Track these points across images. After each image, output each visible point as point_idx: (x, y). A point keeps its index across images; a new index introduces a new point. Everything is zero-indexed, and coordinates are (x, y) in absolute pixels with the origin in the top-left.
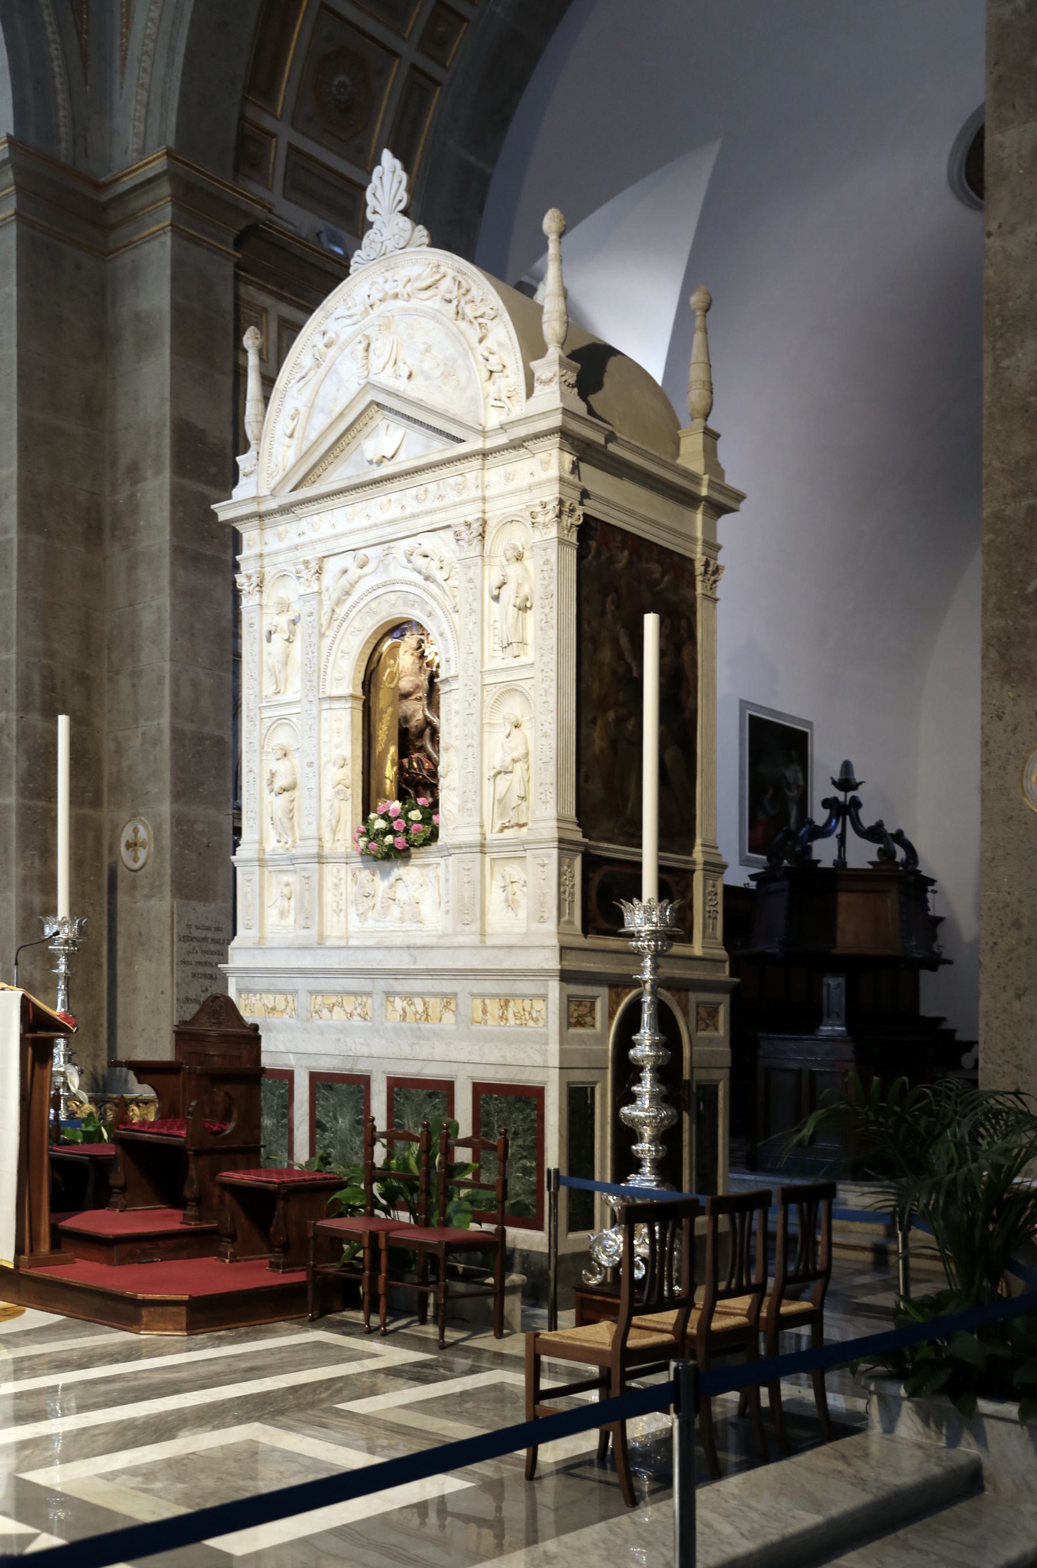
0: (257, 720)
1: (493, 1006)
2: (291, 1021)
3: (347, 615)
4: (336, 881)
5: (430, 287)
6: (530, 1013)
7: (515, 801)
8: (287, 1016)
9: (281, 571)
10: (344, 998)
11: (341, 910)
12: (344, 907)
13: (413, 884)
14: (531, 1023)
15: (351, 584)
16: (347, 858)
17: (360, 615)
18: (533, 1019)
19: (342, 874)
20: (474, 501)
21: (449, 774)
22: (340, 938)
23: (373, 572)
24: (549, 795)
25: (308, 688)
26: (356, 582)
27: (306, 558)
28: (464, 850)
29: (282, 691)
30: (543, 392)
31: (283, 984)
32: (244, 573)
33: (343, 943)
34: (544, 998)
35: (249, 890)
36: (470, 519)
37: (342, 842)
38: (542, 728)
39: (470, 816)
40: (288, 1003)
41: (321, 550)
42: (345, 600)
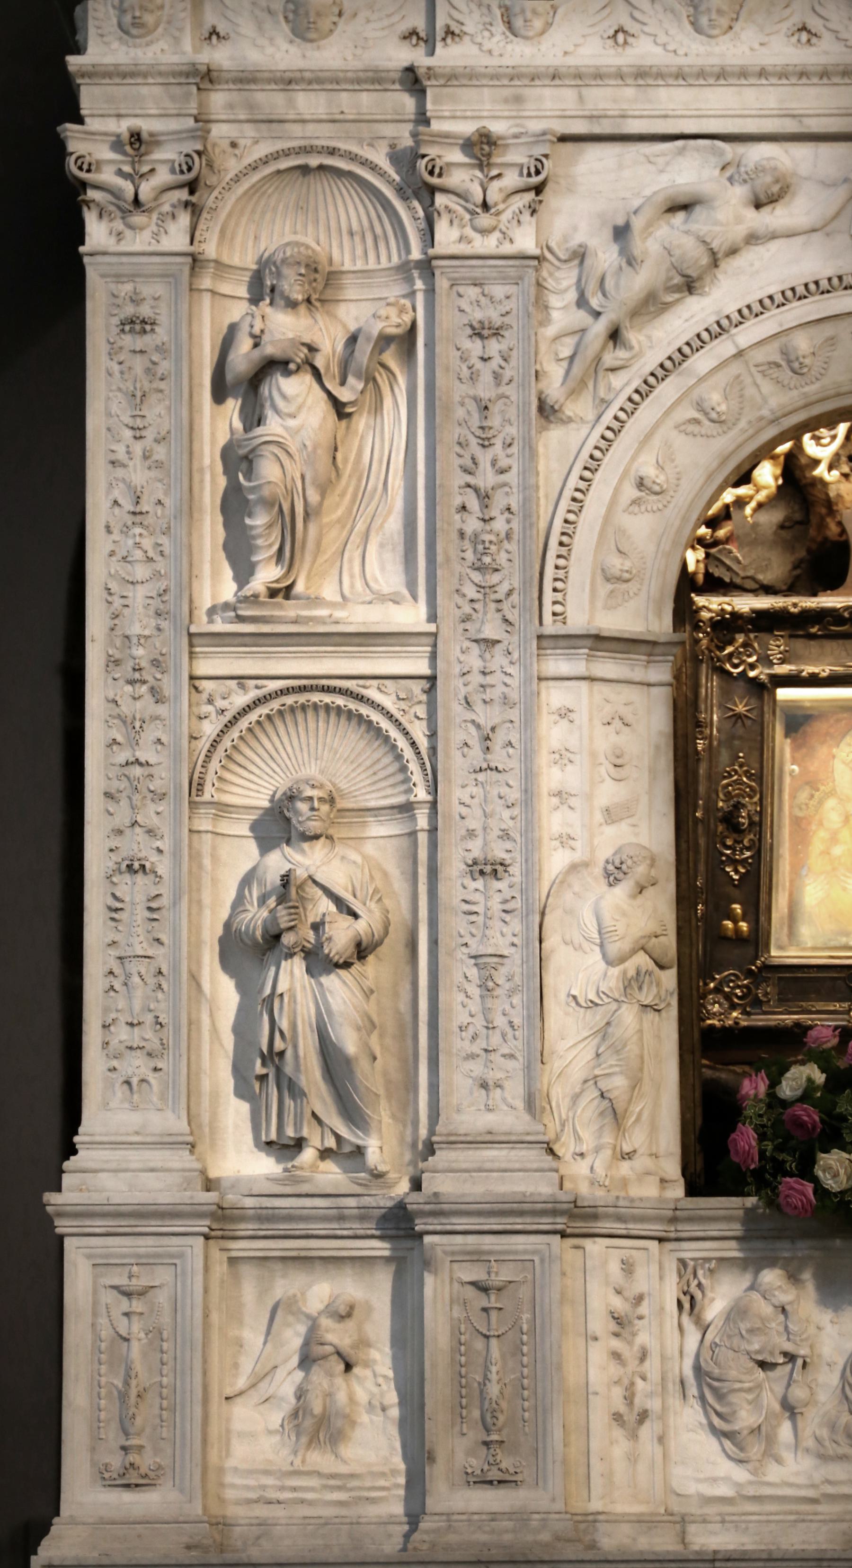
4: (618, 1304)
11: (643, 1416)
12: (654, 1405)
15: (713, 253)
16: (673, 1220)
17: (735, 368)
19: (642, 1282)
25: (471, 592)
26: (733, 251)
27: (146, 126)
32: (93, 124)
42: (666, 307)
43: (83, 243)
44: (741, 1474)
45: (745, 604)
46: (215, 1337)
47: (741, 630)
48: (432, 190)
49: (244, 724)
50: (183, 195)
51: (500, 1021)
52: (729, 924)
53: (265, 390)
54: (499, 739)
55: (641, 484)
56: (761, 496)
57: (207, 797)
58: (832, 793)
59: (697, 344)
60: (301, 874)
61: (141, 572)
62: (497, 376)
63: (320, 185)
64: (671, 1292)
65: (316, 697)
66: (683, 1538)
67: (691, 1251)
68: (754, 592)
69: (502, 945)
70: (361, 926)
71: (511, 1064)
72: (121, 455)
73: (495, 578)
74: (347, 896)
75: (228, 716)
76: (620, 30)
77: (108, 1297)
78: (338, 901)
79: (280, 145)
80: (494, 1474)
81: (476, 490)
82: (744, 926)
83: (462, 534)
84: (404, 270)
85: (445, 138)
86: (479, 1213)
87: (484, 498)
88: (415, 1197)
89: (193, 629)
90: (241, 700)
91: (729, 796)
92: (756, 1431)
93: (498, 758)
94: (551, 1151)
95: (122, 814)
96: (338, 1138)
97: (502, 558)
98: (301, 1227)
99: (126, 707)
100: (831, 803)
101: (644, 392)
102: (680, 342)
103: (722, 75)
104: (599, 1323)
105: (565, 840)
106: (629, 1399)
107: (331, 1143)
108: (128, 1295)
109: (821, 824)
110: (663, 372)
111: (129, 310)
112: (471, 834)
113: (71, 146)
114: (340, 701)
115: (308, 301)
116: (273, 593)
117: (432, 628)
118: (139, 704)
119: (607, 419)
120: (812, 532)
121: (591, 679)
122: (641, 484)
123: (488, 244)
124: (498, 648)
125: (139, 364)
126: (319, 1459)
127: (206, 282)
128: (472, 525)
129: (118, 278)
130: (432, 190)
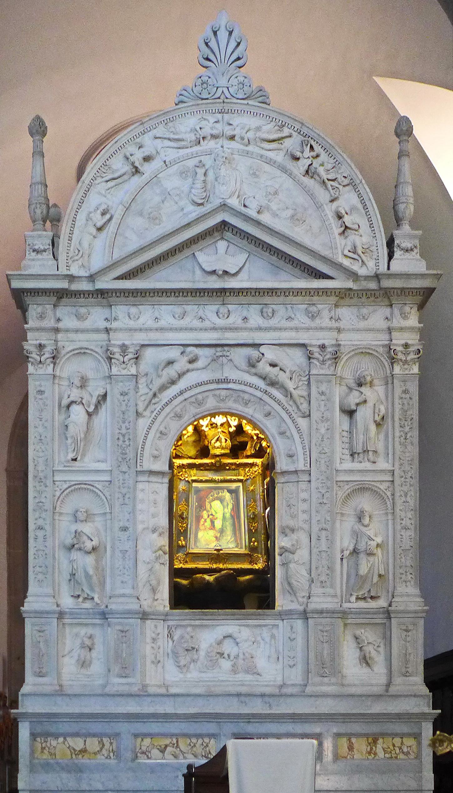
0: (49, 482)
1: (361, 745)
2: (108, 761)
3: (171, 401)
4: (154, 635)
5: (273, 141)
6: (400, 748)
7: (376, 579)
8: (103, 757)
9: (81, 348)
10: (179, 739)
11: (159, 662)
13: (246, 641)
14: (401, 756)
18: (403, 753)
19: (160, 629)
20: (157, 330)
21: (298, 551)
22: (159, 686)
23: (204, 368)
24: (409, 576)
27: (43, 342)
28: (325, 615)
29: (78, 459)
30: (403, 257)
31: (97, 727)
33: (163, 691)
34: (417, 736)
35: (41, 639)
36: (327, 343)
37: (160, 601)
38: (402, 522)
39: (323, 587)
40: (103, 745)
41: (141, 338)
42: (169, 388)
43: (27, 371)
44: (181, 676)
45: (185, 461)
46: (59, 642)
47: (184, 468)
48: (111, 358)
49: (65, 492)
50: (52, 360)
51: (127, 567)
52: (180, 542)
53: (70, 408)
54: (127, 496)
55: (161, 433)
56: (189, 434)
57: (57, 511)
58: (205, 509)
59: (175, 397)
60: (79, 530)
61: (41, 454)
62: (126, 405)
63: (84, 358)
64: (166, 632)
65: (83, 486)
66: (167, 691)
67: (170, 623)
68: (187, 458)
69: (127, 548)
70: (94, 543)
71: (129, 577)
72: (37, 425)
73: (126, 456)
74: (90, 535)
75: (62, 490)
76: (156, 318)
77: (35, 632)
78: (88, 537)
79: (75, 347)
80: (124, 675)
81: (122, 434)
82: (184, 543)
83: (118, 445)
84: (105, 378)
85: (114, 345)
86: (121, 613)
87: (124, 436)
88: (107, 609)
89: (54, 469)
90: (65, 486)
91: (180, 510)
92: (185, 666)
93: (127, 501)
94: (138, 599)
95: (37, 514)
96: (88, 595)
97: (128, 451)
98: (79, 616)
99: (38, 488)
100: (205, 512)
101: (163, 409)
102: (171, 397)
103: (181, 329)
104: (148, 640)
105: (143, 522)
106: (156, 658)
107: (86, 596)
108: (39, 631)
109: (202, 517)
110: (167, 404)
111: (39, 389)
112: (120, 520)
113: (25, 347)
114: (89, 487)
115: (81, 386)
116: (73, 460)
117: (393, 469)
118: (41, 488)
119: (153, 416)
120: (201, 443)
121: (149, 482)
122: (161, 433)
123: (124, 372)
124: (127, 474)
125: (41, 402)
126: (84, 671)
127: (56, 381)
128: (121, 442)
129: (37, 380)
130: (111, 358)
